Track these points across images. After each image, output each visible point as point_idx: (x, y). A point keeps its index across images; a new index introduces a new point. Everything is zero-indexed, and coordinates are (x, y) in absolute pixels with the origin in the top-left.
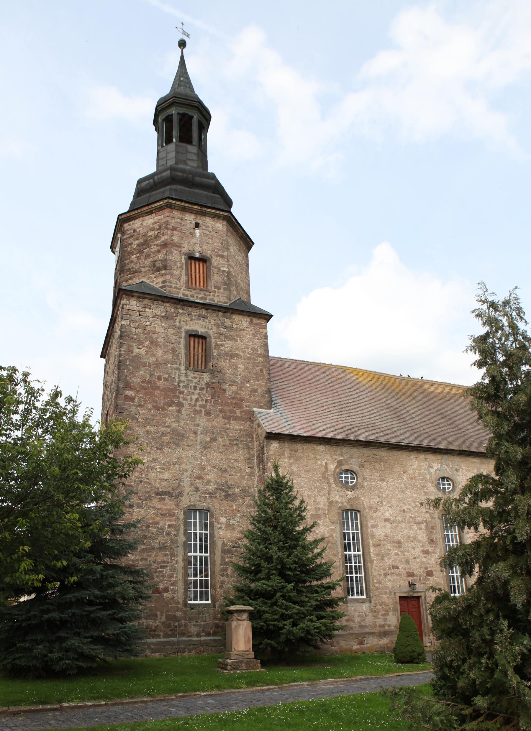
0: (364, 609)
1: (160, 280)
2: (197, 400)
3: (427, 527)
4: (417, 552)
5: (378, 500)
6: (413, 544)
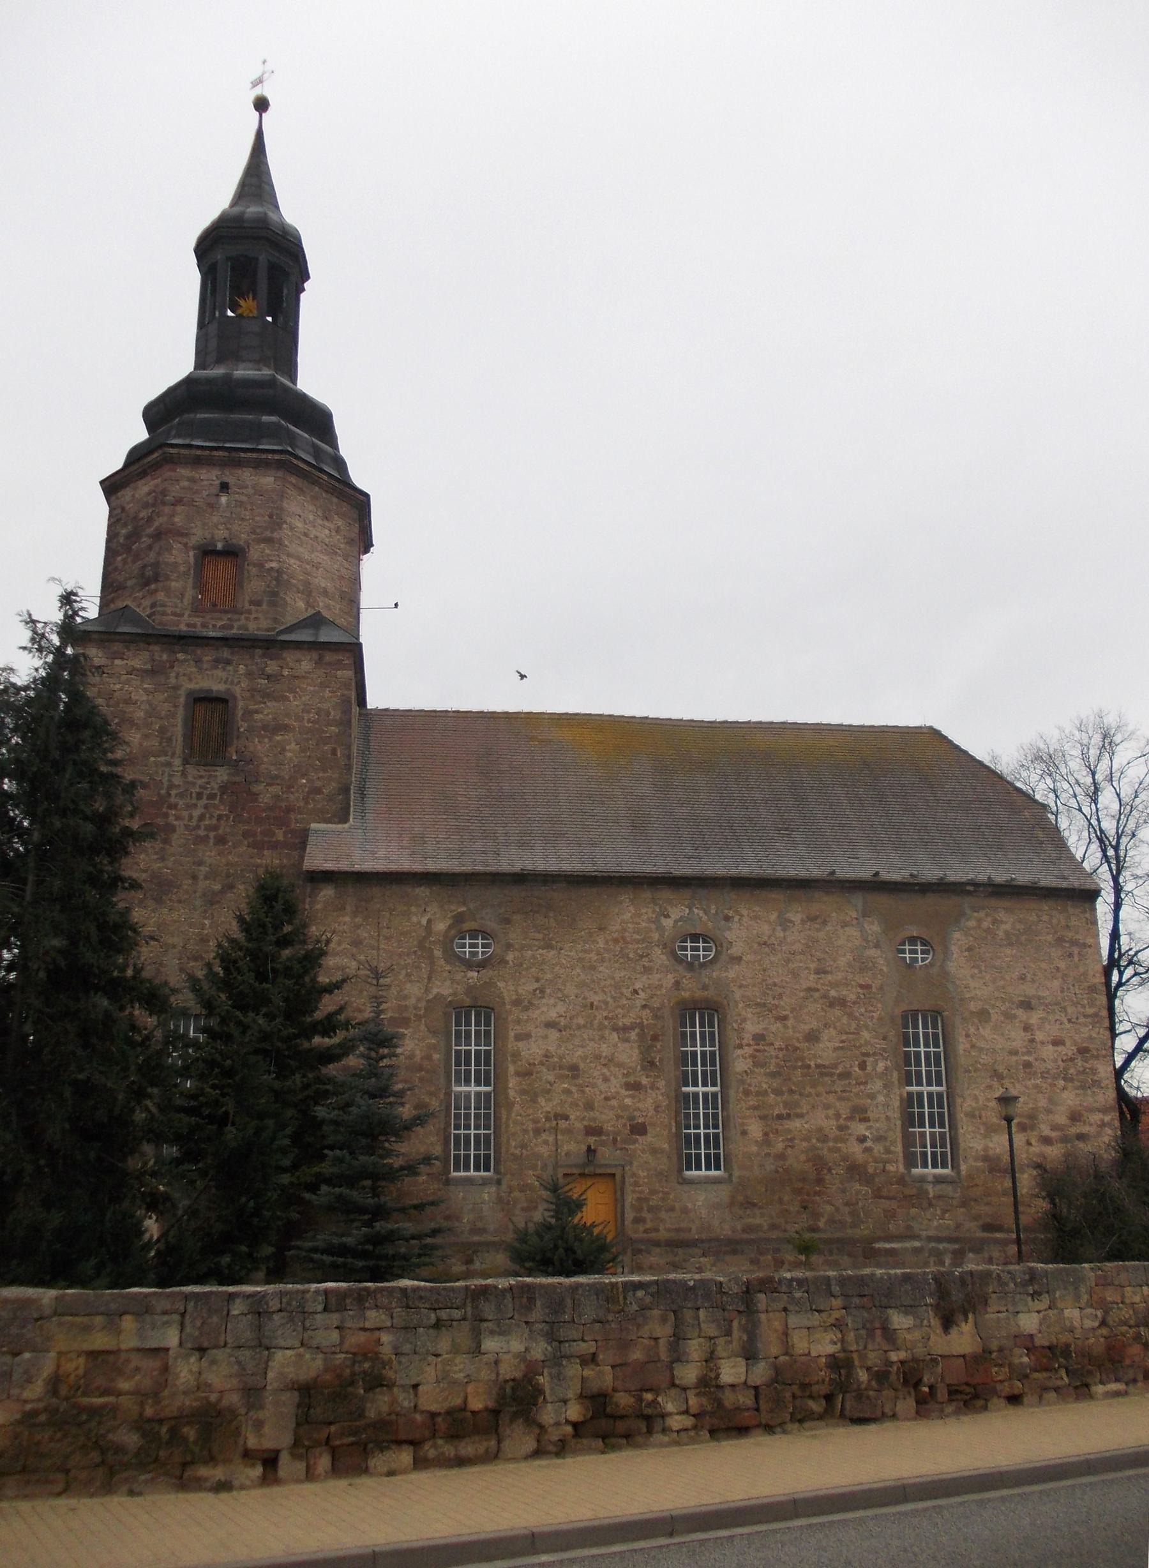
0: (486, 1197)
1: (147, 602)
2: (202, 818)
3: (642, 1036)
4: (615, 1085)
5: (536, 985)
6: (605, 1070)
